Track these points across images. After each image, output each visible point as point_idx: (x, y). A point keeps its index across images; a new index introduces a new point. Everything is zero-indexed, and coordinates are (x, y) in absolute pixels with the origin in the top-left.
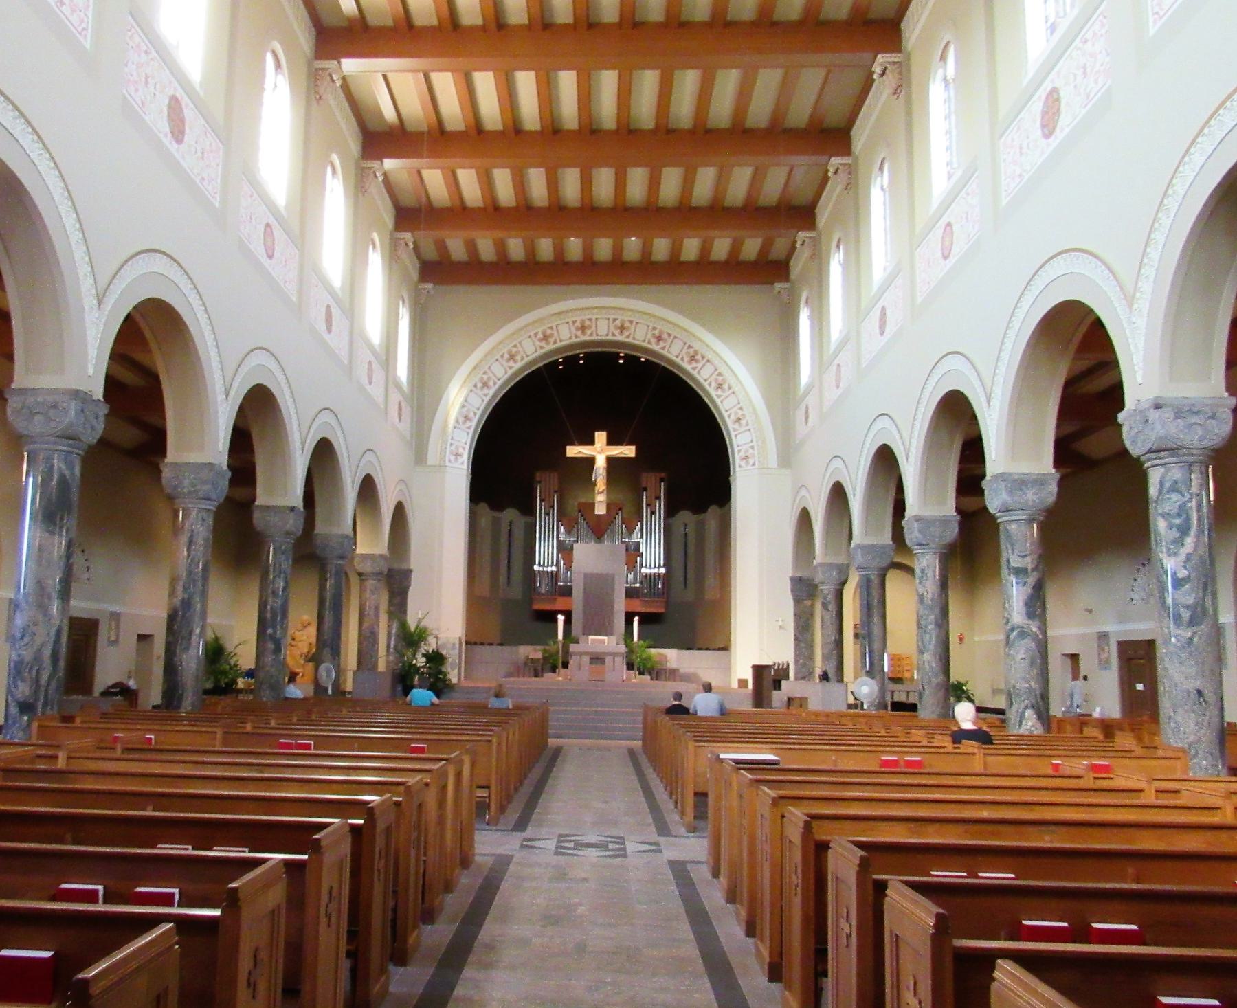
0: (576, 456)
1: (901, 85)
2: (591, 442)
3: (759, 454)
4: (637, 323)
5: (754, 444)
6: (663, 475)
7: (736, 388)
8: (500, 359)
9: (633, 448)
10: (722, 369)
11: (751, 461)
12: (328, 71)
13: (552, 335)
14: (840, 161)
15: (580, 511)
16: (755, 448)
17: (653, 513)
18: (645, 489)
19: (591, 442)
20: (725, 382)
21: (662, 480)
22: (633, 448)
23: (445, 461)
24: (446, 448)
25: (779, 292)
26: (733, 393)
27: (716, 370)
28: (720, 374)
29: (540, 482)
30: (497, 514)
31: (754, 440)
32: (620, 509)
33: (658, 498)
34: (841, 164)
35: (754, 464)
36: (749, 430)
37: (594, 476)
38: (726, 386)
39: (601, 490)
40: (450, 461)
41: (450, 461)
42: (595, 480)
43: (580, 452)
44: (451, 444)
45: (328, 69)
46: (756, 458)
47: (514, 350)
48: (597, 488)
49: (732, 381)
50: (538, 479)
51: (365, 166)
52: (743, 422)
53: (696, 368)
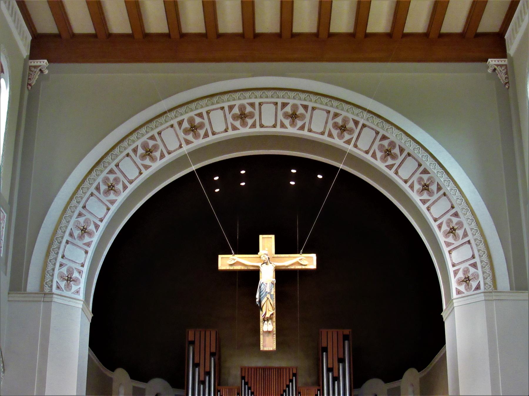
0: (231, 268)
1: (508, 83)
2: (254, 249)
3: (483, 273)
4: (314, 109)
5: (477, 260)
6: (347, 332)
7: (448, 187)
8: (132, 154)
9: (314, 256)
10: (428, 163)
11: (474, 284)
12: (40, 68)
13: (201, 125)
14: (497, 63)
15: (243, 378)
16: (479, 265)
17: (336, 379)
18: (325, 349)
19: (254, 249)
20: (432, 182)
21: (346, 337)
22: (314, 256)
23: (51, 287)
24: (53, 270)
25: (495, 70)
26: (445, 194)
27: (420, 165)
28: (425, 172)
29: (192, 343)
30: (140, 385)
31: (477, 255)
32: (295, 375)
33: (341, 360)
34: (497, 65)
35: (478, 288)
36: (469, 242)
37: (257, 296)
38: (434, 187)
39: (268, 315)
40: (58, 287)
41: (58, 287)
42: (260, 301)
43: (238, 263)
44: (61, 265)
45: (40, 66)
46: (481, 279)
47: (151, 143)
48: (262, 314)
49: (442, 179)
50: (191, 338)
51: (33, 64)
52: (460, 232)
53: (393, 165)
